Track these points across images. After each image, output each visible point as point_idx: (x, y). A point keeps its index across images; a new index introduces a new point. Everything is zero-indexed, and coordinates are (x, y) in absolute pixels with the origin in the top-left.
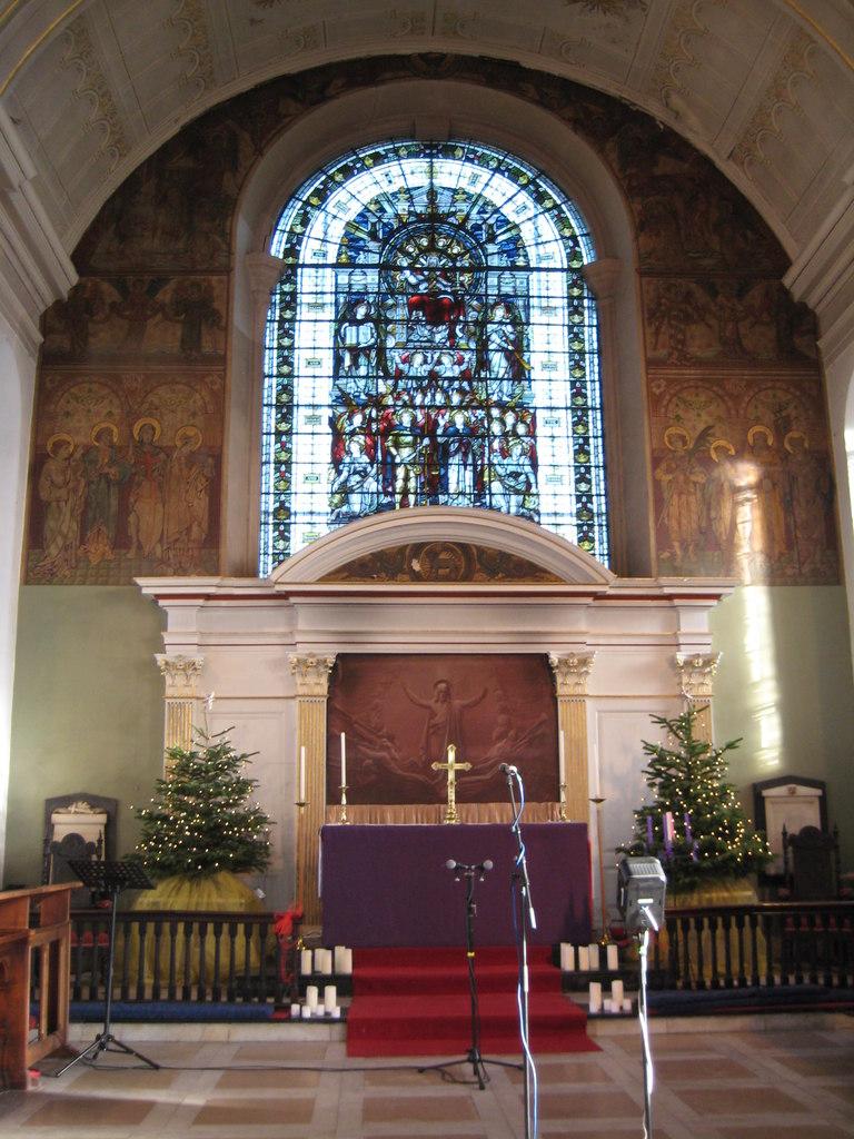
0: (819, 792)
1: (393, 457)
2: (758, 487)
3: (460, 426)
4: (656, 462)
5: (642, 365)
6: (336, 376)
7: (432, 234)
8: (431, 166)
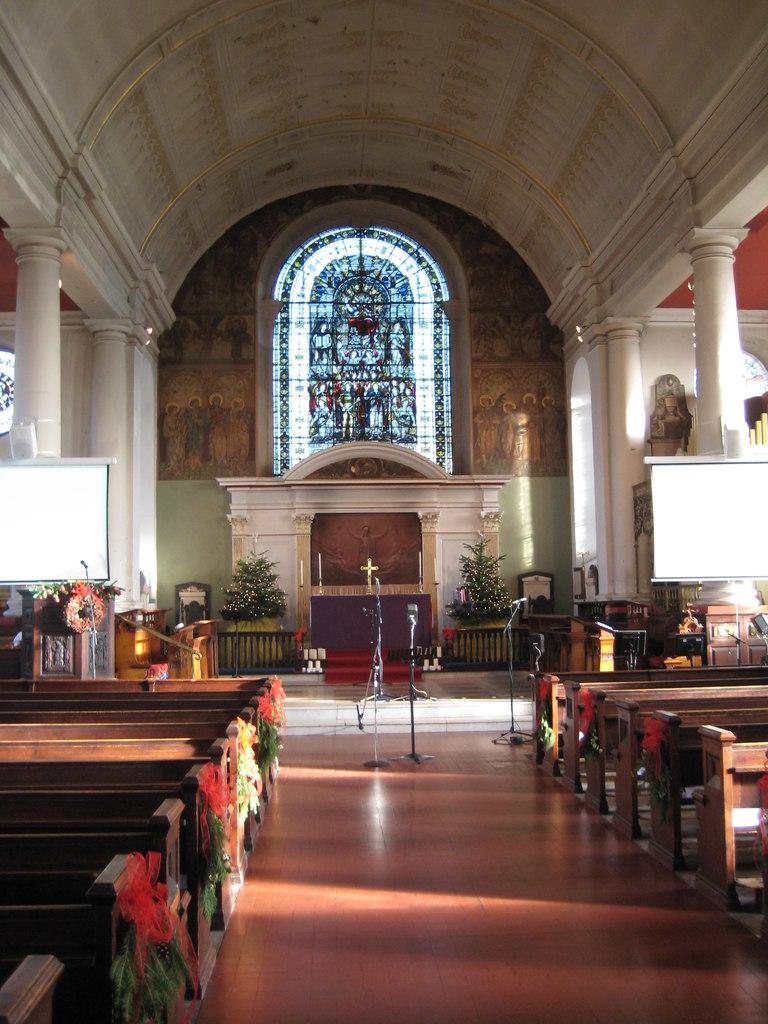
0: (550, 579)
1: (341, 408)
2: (527, 426)
3: (376, 391)
4: (475, 413)
5: (469, 360)
6: (311, 364)
7: (361, 283)
8: (361, 243)
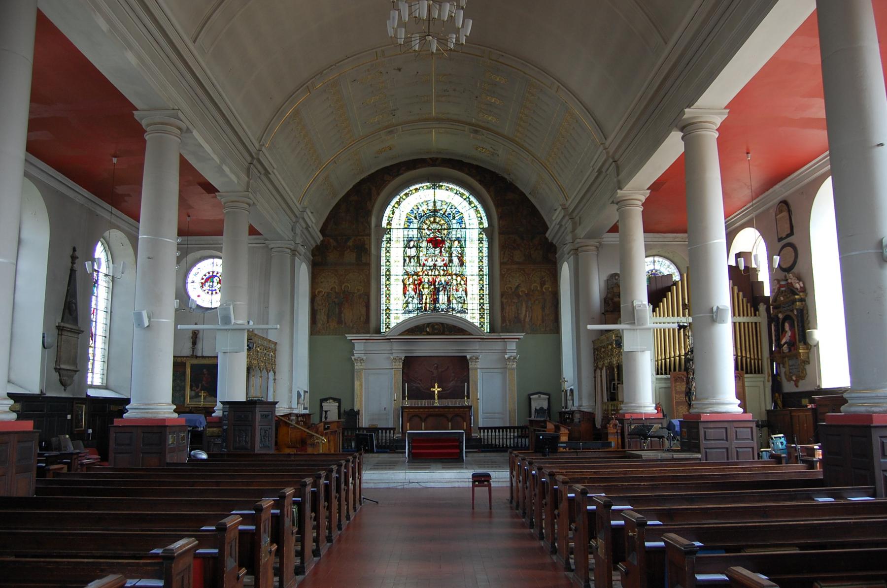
7: (435, 216)
